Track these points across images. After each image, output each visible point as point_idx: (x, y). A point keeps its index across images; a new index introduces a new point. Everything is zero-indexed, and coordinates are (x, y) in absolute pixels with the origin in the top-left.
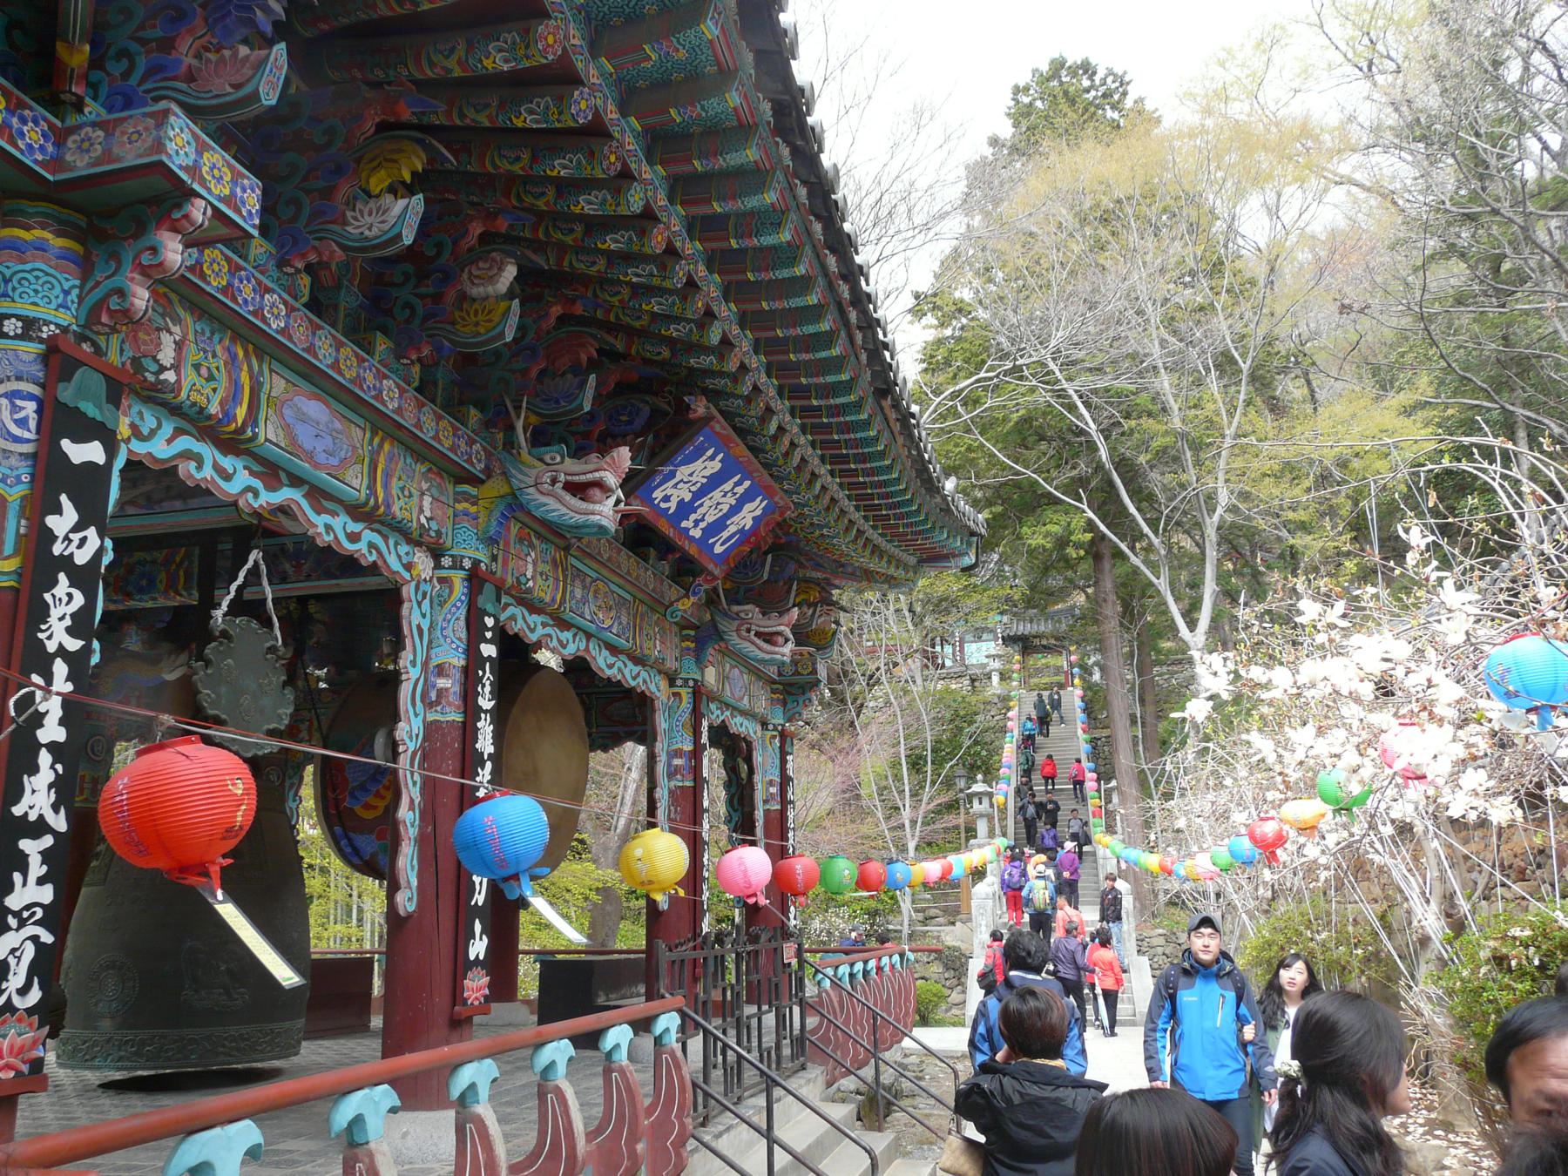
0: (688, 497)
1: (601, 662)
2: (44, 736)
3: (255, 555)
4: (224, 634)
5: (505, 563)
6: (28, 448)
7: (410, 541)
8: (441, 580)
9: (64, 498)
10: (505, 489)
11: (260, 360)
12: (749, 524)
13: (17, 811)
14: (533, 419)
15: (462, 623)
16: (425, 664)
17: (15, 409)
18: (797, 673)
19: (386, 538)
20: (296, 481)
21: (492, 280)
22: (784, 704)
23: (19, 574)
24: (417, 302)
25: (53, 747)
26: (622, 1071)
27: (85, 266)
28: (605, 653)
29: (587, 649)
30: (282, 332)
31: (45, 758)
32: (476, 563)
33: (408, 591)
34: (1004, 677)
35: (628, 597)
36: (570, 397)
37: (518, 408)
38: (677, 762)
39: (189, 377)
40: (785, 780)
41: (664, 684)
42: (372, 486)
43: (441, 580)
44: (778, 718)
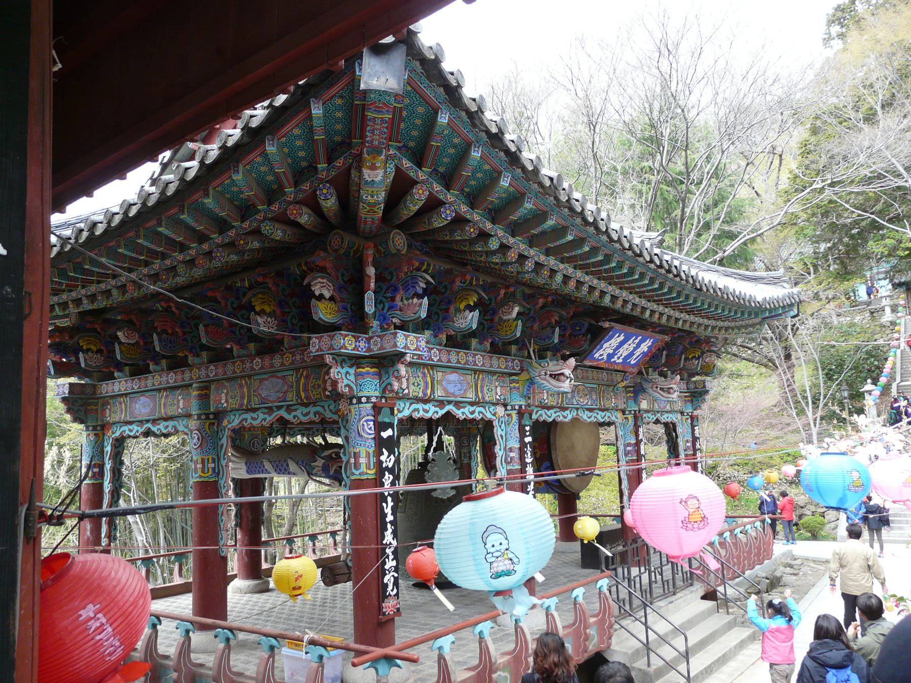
0: (611, 352)
1: (585, 417)
2: (388, 520)
3: (440, 428)
4: (433, 460)
5: (534, 398)
6: (373, 436)
7: (494, 404)
8: (508, 415)
9: (384, 450)
10: (528, 377)
11: (433, 370)
12: (646, 349)
13: (384, 542)
14: (536, 347)
15: (517, 431)
16: (505, 449)
17: (368, 425)
18: (696, 388)
19: (484, 407)
20: (449, 402)
21: (510, 313)
22: (692, 401)
23: (376, 474)
24: (485, 323)
25: (390, 522)
26: (580, 604)
27: (380, 375)
28: (587, 412)
29: (577, 414)
30: (438, 361)
31: (389, 526)
32: (520, 406)
33: (496, 423)
34: (894, 309)
35: (595, 386)
36: (550, 338)
37: (530, 343)
38: (629, 448)
39: (412, 388)
40: (695, 439)
41: (619, 415)
42: (477, 395)
43: (508, 415)
44: (689, 409)
